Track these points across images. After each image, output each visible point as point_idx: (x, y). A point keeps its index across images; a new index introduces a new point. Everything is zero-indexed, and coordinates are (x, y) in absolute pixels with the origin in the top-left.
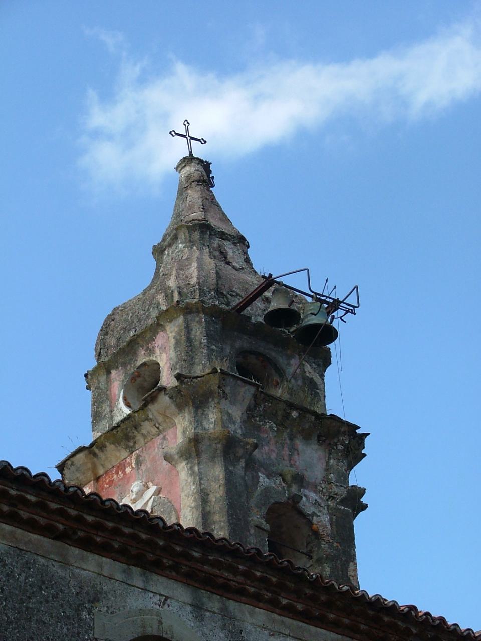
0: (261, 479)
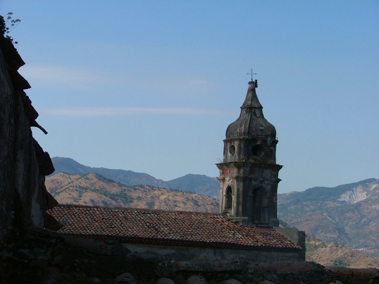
0: (253, 183)
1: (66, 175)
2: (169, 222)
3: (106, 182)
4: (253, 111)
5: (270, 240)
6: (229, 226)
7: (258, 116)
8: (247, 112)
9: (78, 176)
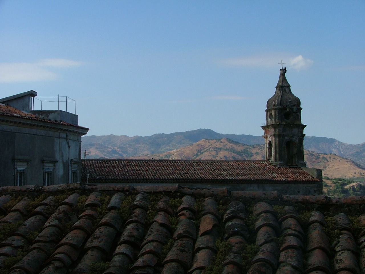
1: (207, 140)
2: (228, 167)
3: (234, 144)
4: (284, 89)
5: (297, 176)
6: (269, 169)
7: (287, 92)
8: (279, 90)
9: (215, 141)
